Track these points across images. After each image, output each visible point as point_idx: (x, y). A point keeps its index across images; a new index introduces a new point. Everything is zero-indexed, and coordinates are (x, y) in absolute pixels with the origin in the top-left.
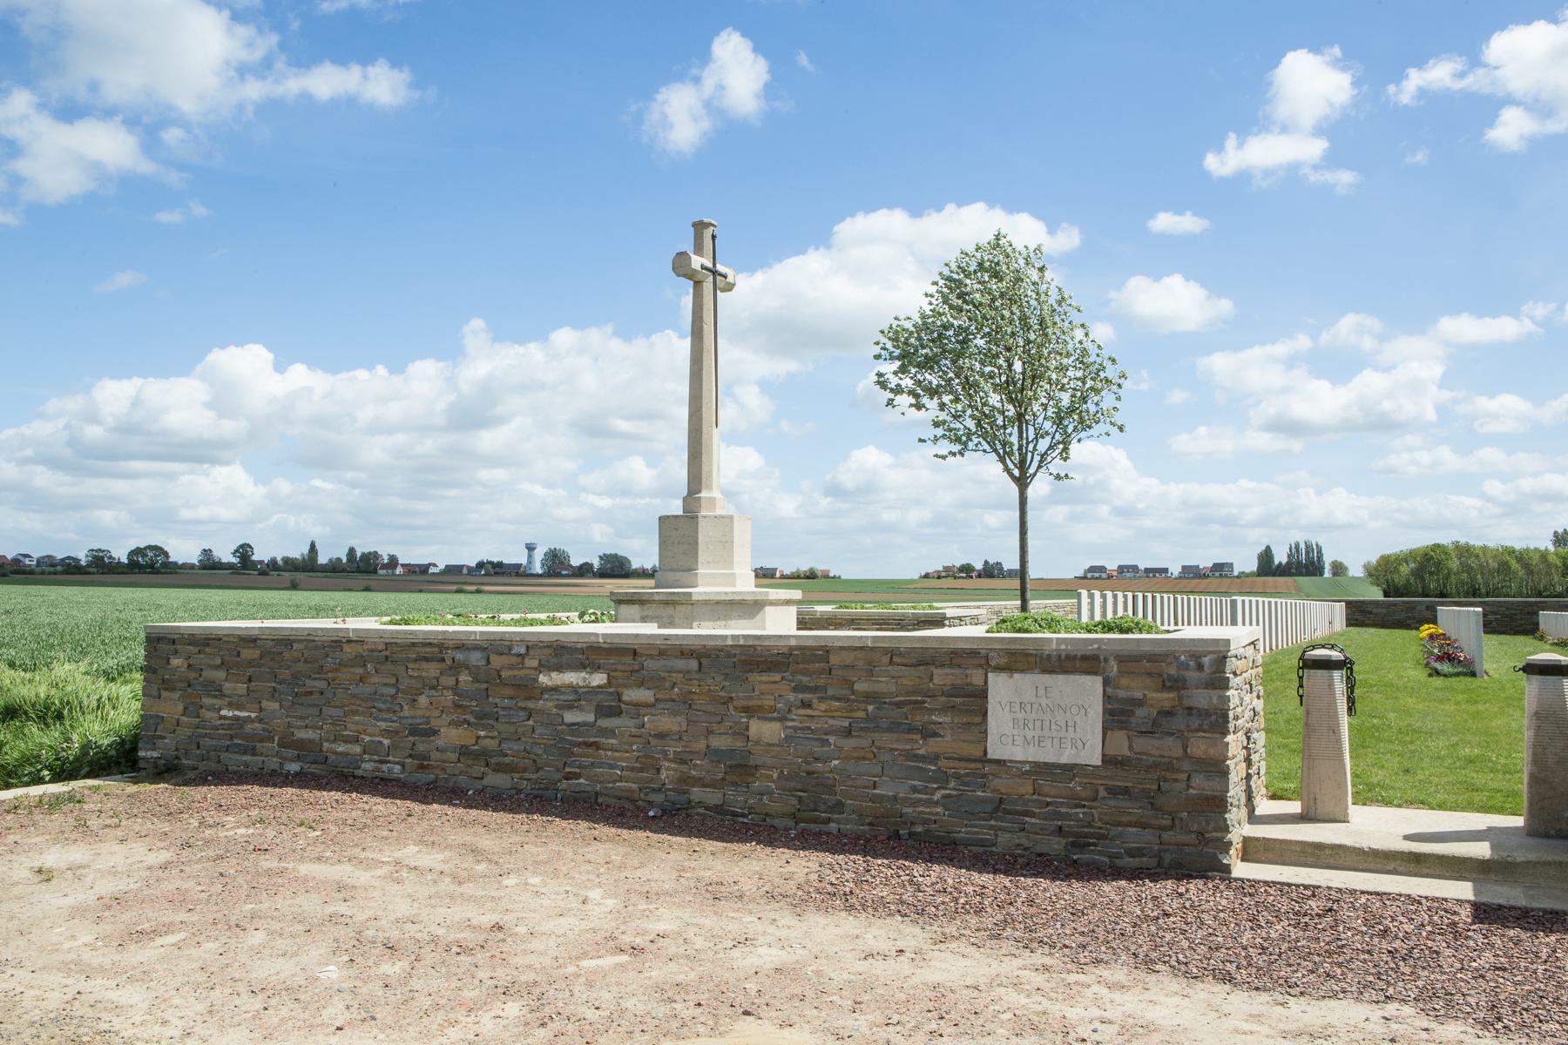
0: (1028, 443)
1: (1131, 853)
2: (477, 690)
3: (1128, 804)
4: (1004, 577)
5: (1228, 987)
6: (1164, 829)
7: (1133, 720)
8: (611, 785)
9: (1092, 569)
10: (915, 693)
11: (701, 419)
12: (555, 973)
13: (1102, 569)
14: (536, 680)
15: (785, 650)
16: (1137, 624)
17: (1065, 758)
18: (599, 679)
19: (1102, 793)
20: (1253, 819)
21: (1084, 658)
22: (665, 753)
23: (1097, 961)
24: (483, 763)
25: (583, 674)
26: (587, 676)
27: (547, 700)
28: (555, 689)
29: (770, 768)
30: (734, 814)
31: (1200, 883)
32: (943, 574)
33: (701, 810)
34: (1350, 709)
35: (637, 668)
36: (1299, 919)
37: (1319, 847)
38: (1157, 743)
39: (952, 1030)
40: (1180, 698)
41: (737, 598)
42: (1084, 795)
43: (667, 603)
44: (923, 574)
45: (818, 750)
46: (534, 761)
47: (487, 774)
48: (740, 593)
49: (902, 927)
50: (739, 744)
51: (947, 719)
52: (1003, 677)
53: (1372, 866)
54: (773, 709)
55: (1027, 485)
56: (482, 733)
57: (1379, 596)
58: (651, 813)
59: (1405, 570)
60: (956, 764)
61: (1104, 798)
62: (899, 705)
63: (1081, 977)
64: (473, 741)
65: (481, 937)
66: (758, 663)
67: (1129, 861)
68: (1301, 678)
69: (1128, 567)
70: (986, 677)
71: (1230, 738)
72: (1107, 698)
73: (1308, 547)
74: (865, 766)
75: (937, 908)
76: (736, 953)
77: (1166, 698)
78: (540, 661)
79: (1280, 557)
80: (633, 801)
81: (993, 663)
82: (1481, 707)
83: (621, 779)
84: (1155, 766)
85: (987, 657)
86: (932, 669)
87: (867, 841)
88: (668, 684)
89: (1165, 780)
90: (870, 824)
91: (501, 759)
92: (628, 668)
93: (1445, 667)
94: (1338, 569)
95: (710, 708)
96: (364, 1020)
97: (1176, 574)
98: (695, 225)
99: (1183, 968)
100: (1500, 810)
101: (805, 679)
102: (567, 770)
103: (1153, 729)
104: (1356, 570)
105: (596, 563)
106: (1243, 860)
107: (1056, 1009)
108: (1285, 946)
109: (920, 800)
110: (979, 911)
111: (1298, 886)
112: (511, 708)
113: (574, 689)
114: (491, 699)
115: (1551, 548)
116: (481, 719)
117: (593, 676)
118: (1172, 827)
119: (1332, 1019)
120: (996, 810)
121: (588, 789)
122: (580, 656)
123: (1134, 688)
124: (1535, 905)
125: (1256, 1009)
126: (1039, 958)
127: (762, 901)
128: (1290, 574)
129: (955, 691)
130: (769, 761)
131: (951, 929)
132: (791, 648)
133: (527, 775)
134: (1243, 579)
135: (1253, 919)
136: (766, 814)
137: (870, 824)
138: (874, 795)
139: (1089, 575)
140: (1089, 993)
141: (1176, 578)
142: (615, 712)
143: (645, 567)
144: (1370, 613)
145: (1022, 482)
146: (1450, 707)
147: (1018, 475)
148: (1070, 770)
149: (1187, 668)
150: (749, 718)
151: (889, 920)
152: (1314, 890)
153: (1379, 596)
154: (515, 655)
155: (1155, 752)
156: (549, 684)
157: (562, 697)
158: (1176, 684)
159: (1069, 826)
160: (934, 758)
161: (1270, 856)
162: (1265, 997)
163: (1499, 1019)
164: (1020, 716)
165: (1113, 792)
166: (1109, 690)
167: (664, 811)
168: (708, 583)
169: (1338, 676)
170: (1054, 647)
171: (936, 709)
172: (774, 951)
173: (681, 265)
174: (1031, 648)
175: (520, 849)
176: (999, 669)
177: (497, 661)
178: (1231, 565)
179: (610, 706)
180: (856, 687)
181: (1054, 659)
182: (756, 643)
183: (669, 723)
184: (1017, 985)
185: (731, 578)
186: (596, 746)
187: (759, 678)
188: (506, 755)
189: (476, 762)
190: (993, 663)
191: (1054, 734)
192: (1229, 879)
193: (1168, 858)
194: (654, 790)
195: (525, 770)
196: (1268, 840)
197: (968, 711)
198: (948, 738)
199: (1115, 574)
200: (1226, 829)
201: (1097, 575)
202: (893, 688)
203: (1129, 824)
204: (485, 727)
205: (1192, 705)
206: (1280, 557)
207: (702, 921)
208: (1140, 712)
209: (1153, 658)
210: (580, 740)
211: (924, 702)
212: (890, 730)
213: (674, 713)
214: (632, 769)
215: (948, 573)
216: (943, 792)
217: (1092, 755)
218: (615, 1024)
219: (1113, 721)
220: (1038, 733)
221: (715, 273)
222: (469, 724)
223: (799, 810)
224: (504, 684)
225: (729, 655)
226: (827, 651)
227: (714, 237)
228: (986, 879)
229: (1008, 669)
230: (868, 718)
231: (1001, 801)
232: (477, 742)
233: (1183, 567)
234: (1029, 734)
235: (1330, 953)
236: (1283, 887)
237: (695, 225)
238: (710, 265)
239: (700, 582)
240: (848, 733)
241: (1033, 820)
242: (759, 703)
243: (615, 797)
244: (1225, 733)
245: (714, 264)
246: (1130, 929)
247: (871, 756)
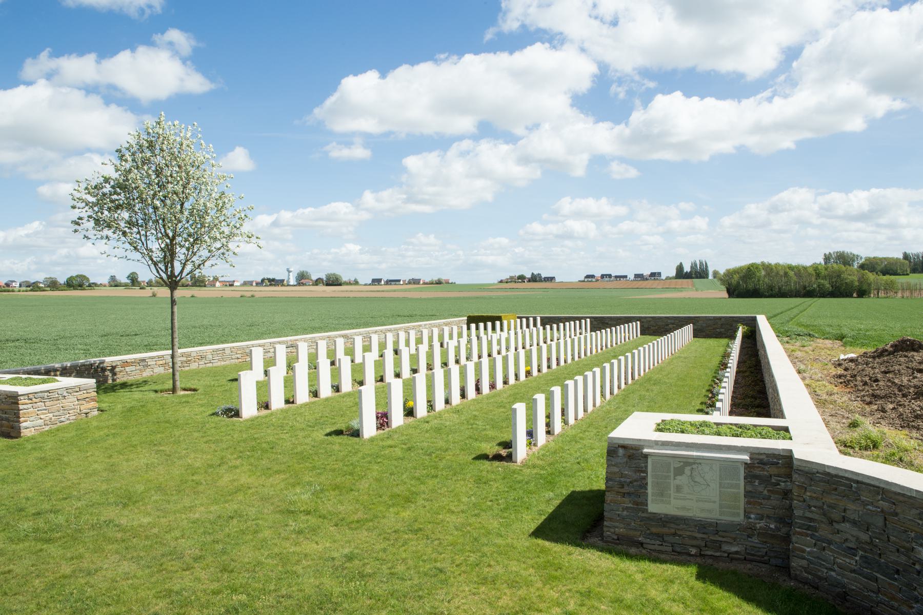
9: (588, 277)
13: (593, 276)
44: (499, 280)
59: (736, 277)
73: (701, 263)
79: (687, 269)
115: (823, 262)
199: (599, 278)
201: (590, 279)
206: (687, 269)
233: (635, 275)
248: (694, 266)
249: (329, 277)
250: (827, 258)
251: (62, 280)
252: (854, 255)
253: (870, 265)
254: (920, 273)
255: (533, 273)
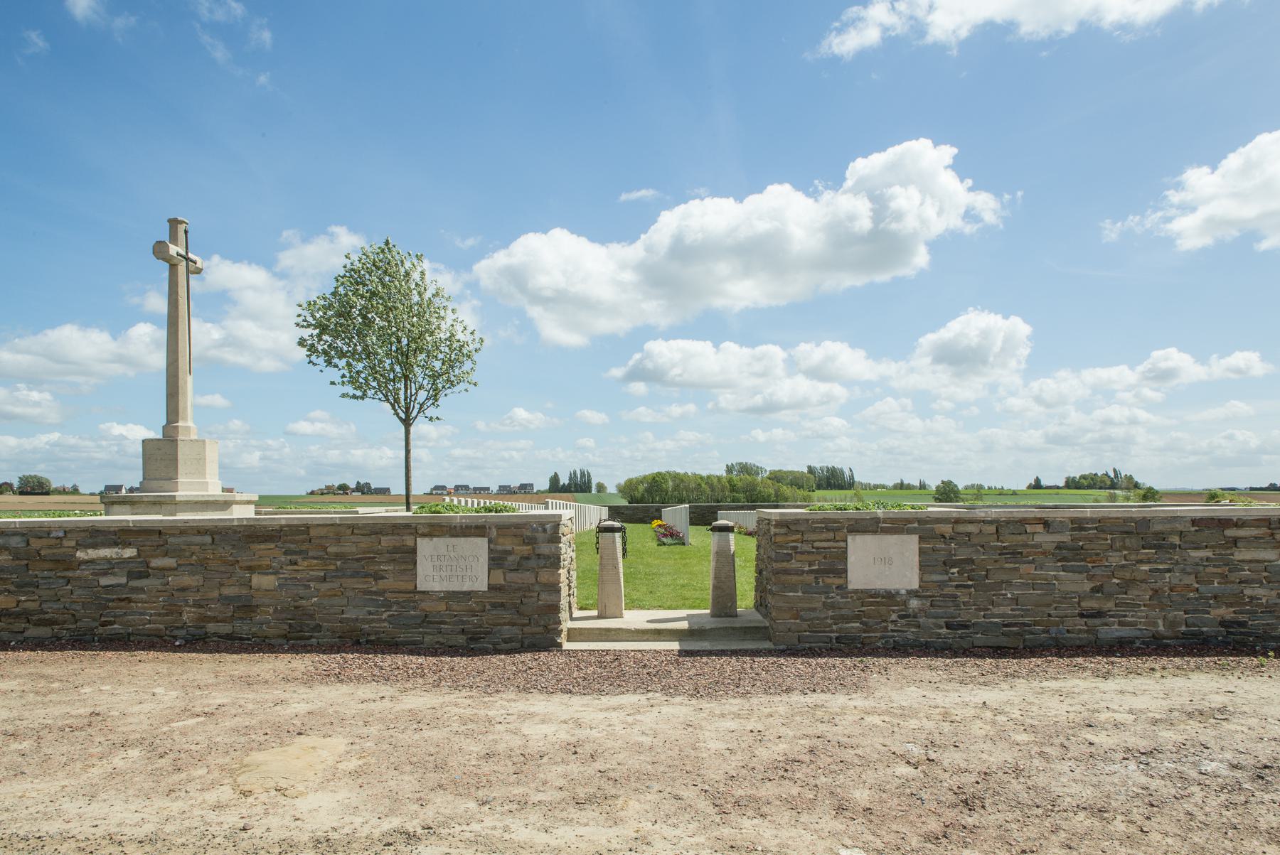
0: (411, 396)
1: (505, 641)
2: (17, 565)
3: (504, 613)
4: (372, 493)
5: (569, 695)
6: (524, 625)
7: (506, 563)
8: (141, 627)
9: (437, 488)
10: (369, 552)
11: (178, 368)
12: (155, 732)
13: (443, 488)
14: (74, 556)
15: (277, 528)
16: (506, 507)
17: (466, 587)
18: (130, 552)
19: (488, 607)
20: (572, 619)
21: (477, 527)
22: (186, 601)
23: (498, 691)
24: (25, 621)
25: (116, 550)
26: (119, 551)
27: (84, 570)
28: (92, 561)
29: (268, 606)
30: (241, 639)
31: (546, 653)
32: (325, 491)
33: (215, 639)
34: (624, 554)
35: (161, 543)
36: (601, 664)
37: (608, 630)
38: (520, 576)
39: (427, 727)
40: (534, 549)
41: (211, 499)
42: (477, 609)
43: (154, 503)
44: (309, 491)
45: (302, 592)
46: (73, 615)
47: (28, 628)
48: (214, 495)
49: (378, 687)
50: (244, 591)
51: (391, 568)
52: (426, 540)
53: (636, 638)
54: (269, 567)
55: (411, 425)
56: (23, 598)
57: (627, 504)
58: (177, 643)
59: (641, 488)
60: (397, 595)
61: (489, 610)
62: (358, 560)
63: (491, 699)
64: (15, 605)
65: (86, 721)
66: (257, 537)
67: (504, 646)
68: (597, 538)
69: (462, 487)
70: (416, 540)
71: (561, 571)
72: (490, 551)
73: (583, 474)
74: (336, 600)
75: (396, 676)
76: (278, 708)
77: (526, 549)
78: (77, 541)
79: (564, 480)
80: (161, 637)
81: (420, 532)
82: (688, 561)
83: (150, 622)
84: (519, 589)
85: (416, 528)
86: (380, 536)
87: (339, 647)
88: (187, 554)
89: (525, 597)
90: (339, 637)
91: (42, 616)
92: (155, 544)
93: (668, 540)
94: (601, 488)
95: (222, 569)
96: (15, 775)
97: (495, 491)
98: (169, 221)
99: (545, 690)
100: (698, 607)
101: (292, 546)
102: (103, 619)
103: (518, 568)
104: (611, 489)
105: (16, 483)
106: (567, 641)
107: (482, 712)
108: (596, 676)
109: (373, 620)
110: (423, 676)
111: (598, 651)
112: (50, 578)
113: (108, 560)
114: (30, 572)
115: (725, 474)
116: (22, 587)
117: (125, 551)
118: (529, 624)
119: (623, 702)
120: (423, 622)
121: (121, 631)
122: (113, 537)
123: (506, 544)
124: (715, 648)
125: (585, 702)
126: (464, 693)
127: (282, 683)
128: (570, 492)
129: (395, 550)
130: (266, 601)
131: (409, 685)
132: (282, 526)
133: (66, 626)
134: (540, 495)
135: (578, 666)
136: (266, 637)
137: (339, 637)
138: (342, 618)
139: (434, 492)
140: (498, 704)
141: (495, 494)
142: (143, 575)
143: (66, 486)
144: (623, 513)
145: (407, 422)
146: (671, 562)
147: (404, 417)
148: (469, 595)
149: (537, 531)
150: (251, 573)
151: (368, 685)
152: (607, 652)
153: (627, 504)
154: (53, 538)
155: (520, 581)
156: (86, 558)
157: (98, 567)
158: (531, 541)
159: (469, 628)
160: (382, 593)
161: (582, 637)
162: (589, 697)
163: (698, 692)
164: (438, 563)
165: (494, 606)
166: (492, 546)
167: (187, 642)
168: (186, 489)
169: (618, 536)
170: (458, 521)
171: (383, 562)
172: (302, 705)
173: (160, 250)
174: (444, 522)
175: (82, 672)
176: (424, 535)
177: (35, 544)
178: (532, 485)
179: (139, 571)
180: (329, 550)
181: (458, 528)
182: (256, 523)
183: (187, 580)
184: (456, 705)
185: (205, 485)
186: (129, 600)
187: (259, 547)
188: (47, 613)
189: (17, 620)
190: (420, 532)
191: (459, 573)
192: (561, 651)
193: (526, 642)
194: (177, 628)
195: (65, 622)
196: (581, 628)
197: (405, 562)
198: (391, 580)
199: (453, 491)
200: (559, 623)
201: (439, 492)
202: (354, 549)
203: (505, 624)
204: (25, 594)
205: (540, 553)
206: (564, 480)
207: (246, 696)
208: (510, 558)
209: (517, 526)
210: (114, 597)
211: (375, 558)
212: (352, 576)
213: (192, 573)
214: (159, 615)
215: (329, 490)
216: (388, 613)
217: (482, 585)
218: (214, 749)
219: (494, 564)
220: (449, 573)
221: (187, 259)
222: (9, 592)
223: (289, 632)
224: (43, 559)
225: (235, 532)
226: (308, 528)
227: (186, 232)
228: (421, 660)
229: (430, 535)
230: (337, 570)
231: (426, 616)
232: (17, 605)
233: (500, 487)
234: (443, 574)
235: (618, 677)
236: (592, 652)
237: (169, 221)
238: (184, 253)
239: (179, 488)
240: (324, 579)
241: (446, 627)
242: (259, 563)
243: (144, 635)
244: (559, 568)
245: (187, 253)
246: (512, 676)
247: (340, 593)
248: (573, 477)
249: (25, 481)
250: (730, 469)
251: (451, 486)
252: (757, 467)
253: (777, 477)
254: (824, 489)
255: (358, 482)
